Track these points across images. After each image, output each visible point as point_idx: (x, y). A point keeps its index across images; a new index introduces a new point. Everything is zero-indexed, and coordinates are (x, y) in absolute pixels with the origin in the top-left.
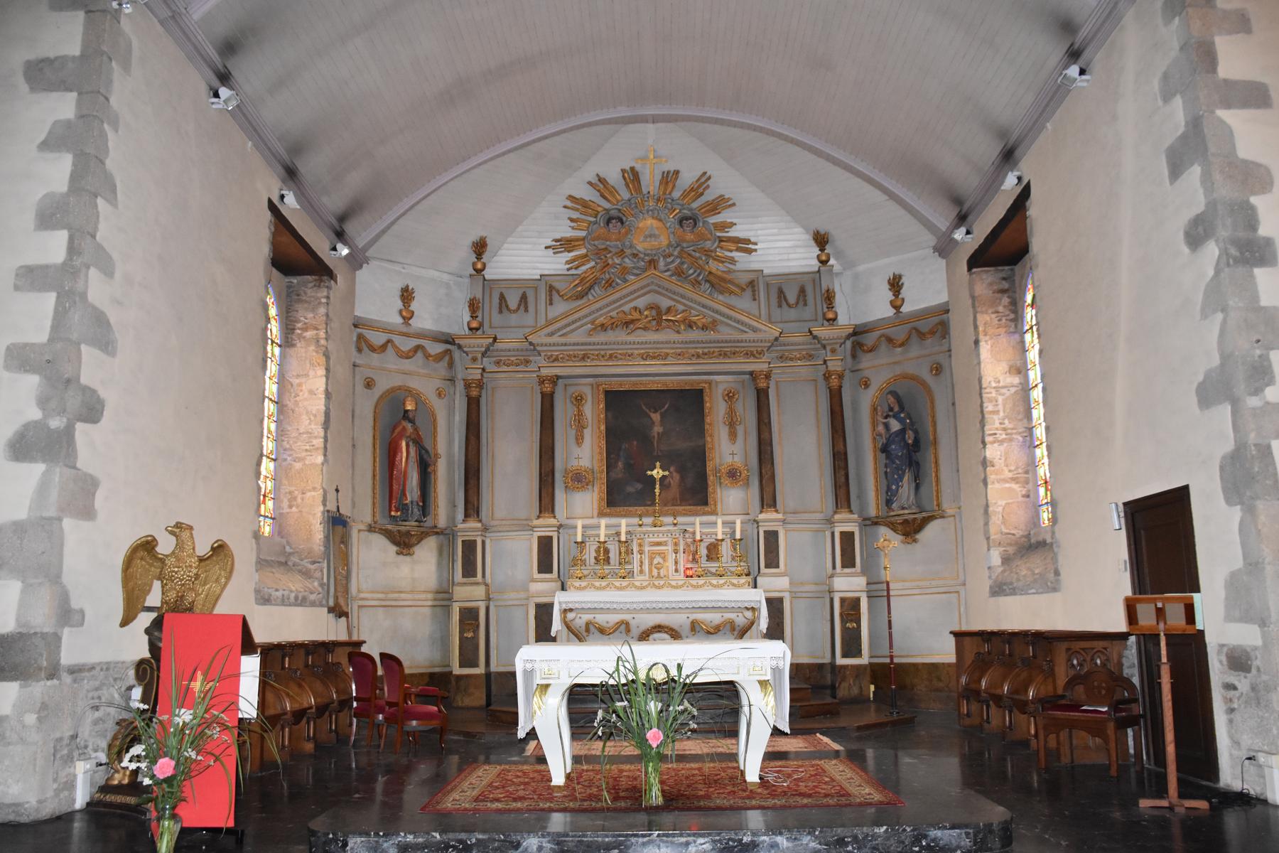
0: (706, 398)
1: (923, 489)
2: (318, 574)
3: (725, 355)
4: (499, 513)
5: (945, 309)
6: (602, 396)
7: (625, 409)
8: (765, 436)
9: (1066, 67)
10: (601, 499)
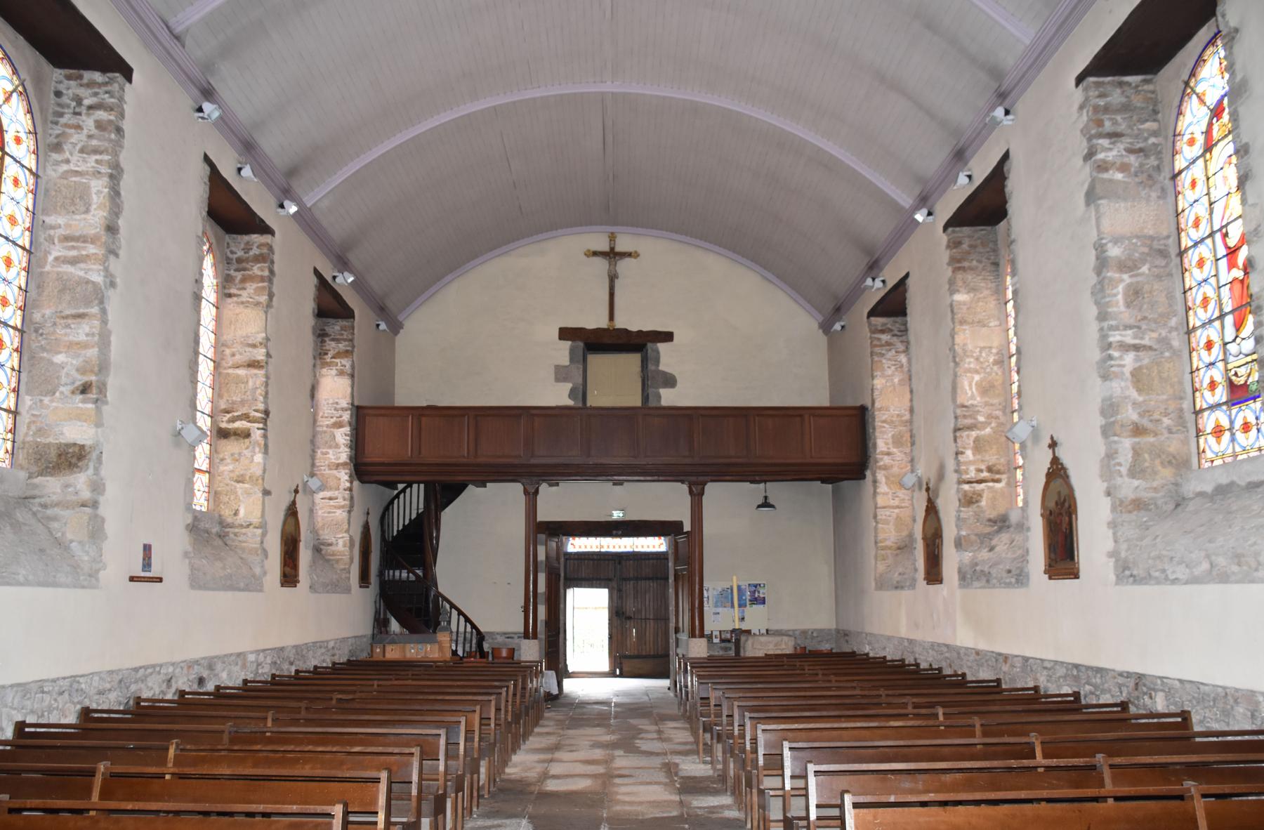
9: (993, 108)
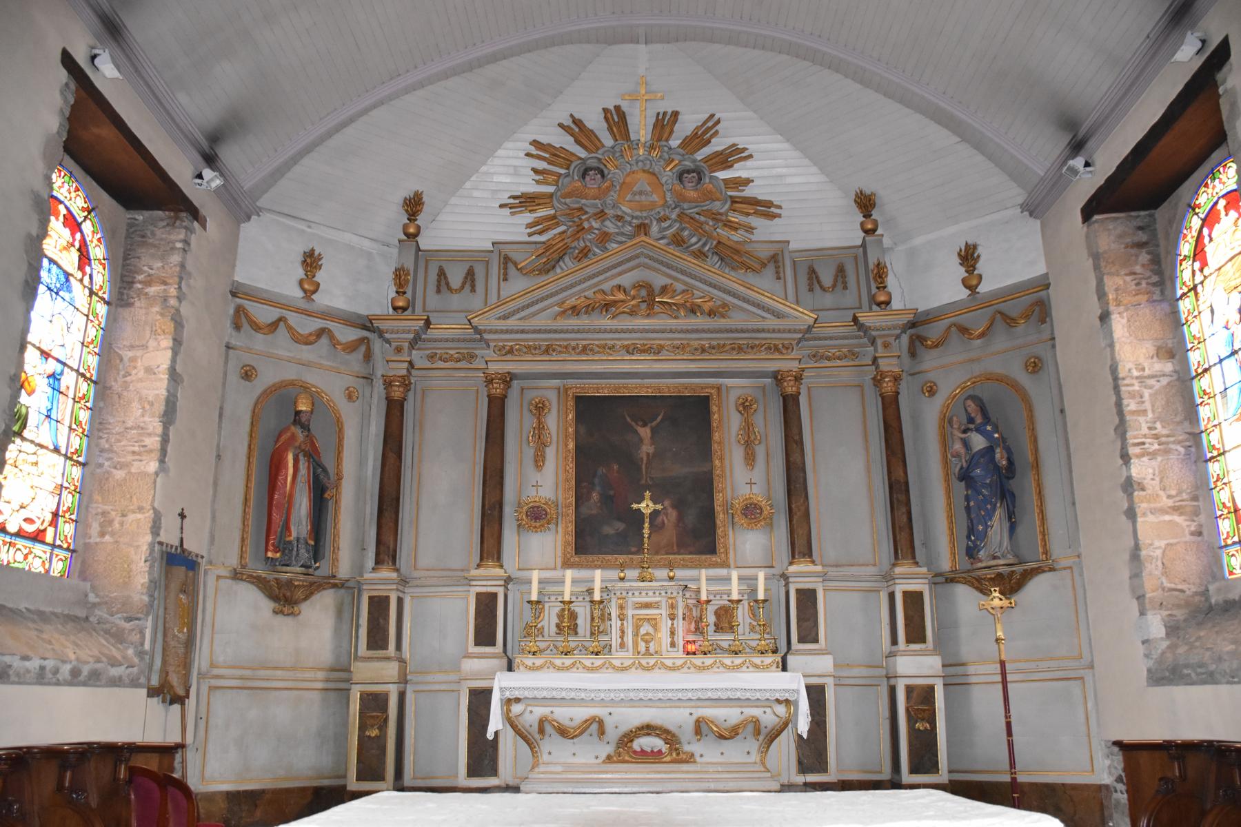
0: (714, 408)
1: (1021, 531)
2: (135, 637)
3: (740, 349)
4: (425, 560)
5: (1043, 284)
6: (571, 403)
7: (601, 422)
8: (796, 457)
10: (566, 544)
